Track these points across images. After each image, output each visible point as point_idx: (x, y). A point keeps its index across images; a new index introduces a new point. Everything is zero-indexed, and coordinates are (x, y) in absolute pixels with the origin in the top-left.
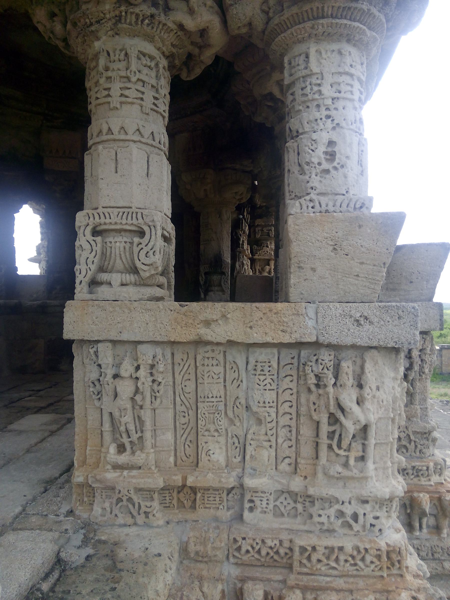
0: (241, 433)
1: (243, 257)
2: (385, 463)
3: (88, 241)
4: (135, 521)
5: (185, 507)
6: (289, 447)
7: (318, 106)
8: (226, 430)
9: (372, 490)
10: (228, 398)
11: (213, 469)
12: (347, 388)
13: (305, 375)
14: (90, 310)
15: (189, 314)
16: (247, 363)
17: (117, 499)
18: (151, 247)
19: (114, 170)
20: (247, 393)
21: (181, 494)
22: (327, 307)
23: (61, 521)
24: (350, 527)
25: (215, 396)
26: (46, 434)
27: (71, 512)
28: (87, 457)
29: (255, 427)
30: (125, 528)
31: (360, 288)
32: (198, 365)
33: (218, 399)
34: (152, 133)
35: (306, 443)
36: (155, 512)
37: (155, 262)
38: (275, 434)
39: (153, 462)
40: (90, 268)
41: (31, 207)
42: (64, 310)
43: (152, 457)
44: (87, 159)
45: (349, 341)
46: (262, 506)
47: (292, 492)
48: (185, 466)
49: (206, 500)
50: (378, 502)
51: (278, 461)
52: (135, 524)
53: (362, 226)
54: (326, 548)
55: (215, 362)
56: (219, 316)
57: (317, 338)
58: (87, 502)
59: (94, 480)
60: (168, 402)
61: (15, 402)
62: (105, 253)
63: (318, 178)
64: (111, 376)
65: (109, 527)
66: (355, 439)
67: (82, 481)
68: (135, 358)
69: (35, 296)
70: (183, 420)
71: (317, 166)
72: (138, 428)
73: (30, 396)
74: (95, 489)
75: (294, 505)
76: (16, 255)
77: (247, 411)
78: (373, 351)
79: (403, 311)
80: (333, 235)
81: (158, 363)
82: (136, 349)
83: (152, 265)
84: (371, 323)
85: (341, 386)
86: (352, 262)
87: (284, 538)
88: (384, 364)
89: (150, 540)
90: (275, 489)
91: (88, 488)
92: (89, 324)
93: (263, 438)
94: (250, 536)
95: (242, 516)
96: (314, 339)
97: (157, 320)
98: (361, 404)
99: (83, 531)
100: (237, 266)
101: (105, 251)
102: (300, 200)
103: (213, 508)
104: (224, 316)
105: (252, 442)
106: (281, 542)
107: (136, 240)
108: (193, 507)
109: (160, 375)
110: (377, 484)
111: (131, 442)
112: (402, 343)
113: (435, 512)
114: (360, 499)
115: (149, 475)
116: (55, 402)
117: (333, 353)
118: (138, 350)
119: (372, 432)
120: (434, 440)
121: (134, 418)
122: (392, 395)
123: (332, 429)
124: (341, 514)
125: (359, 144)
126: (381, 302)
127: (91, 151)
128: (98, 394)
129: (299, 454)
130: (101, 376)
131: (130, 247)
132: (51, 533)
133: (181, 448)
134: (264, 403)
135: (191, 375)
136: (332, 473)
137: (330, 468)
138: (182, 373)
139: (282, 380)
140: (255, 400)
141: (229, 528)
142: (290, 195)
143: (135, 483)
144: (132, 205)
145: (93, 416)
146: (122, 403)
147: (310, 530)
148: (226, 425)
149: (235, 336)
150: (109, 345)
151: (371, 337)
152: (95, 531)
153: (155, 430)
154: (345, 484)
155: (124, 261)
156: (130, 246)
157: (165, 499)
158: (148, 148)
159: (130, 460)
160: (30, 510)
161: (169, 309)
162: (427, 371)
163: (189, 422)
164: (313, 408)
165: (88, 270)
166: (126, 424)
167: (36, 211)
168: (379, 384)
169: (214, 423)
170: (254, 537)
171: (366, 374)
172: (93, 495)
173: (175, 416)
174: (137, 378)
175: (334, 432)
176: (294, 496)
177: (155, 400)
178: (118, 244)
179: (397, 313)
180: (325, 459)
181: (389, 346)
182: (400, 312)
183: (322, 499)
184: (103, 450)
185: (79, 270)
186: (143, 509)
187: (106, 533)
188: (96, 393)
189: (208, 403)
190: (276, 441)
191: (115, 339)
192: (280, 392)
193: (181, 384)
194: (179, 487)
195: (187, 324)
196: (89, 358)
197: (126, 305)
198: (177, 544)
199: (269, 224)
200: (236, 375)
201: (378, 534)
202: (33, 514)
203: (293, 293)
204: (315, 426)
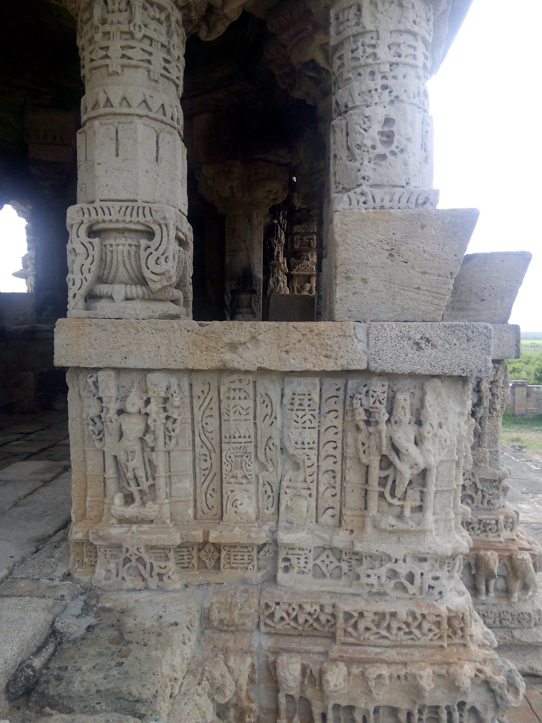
0: (274, 480)
1: (278, 272)
2: (447, 514)
4: (147, 584)
5: (206, 567)
6: (333, 496)
7: (372, 73)
9: (433, 546)
10: (259, 438)
11: (241, 522)
12: (404, 425)
13: (353, 410)
15: (210, 335)
16: (282, 396)
20: (282, 432)
23: (56, 586)
24: (405, 589)
25: (242, 436)
26: (38, 484)
27: (68, 576)
29: (291, 472)
31: (421, 304)
32: (222, 398)
33: (247, 440)
36: (170, 574)
37: (168, 271)
39: (168, 515)
40: (85, 277)
43: (166, 509)
44: (80, 138)
45: (406, 368)
46: (299, 565)
47: (336, 548)
48: (207, 519)
50: (439, 559)
52: (147, 588)
53: (426, 226)
54: (375, 614)
55: (243, 395)
58: (88, 563)
59: (96, 536)
60: (185, 442)
62: (104, 259)
63: (372, 165)
65: (115, 592)
66: (411, 486)
67: (82, 538)
68: (144, 389)
70: (204, 465)
71: (370, 150)
73: (18, 440)
74: (98, 548)
75: (338, 564)
77: (282, 453)
78: (435, 380)
79: (473, 332)
80: (389, 237)
81: (172, 395)
82: (146, 378)
83: (164, 274)
84: (434, 346)
85: (396, 422)
86: (412, 271)
87: (326, 603)
88: (448, 397)
89: (165, 606)
90: (315, 545)
91: (89, 547)
92: (86, 348)
93: (300, 485)
94: (285, 600)
95: (275, 577)
96: (364, 366)
98: (419, 444)
99: (83, 597)
100: (271, 282)
101: (104, 256)
102: (349, 193)
103: (241, 568)
105: (287, 490)
106: (322, 607)
107: (144, 242)
108: (217, 567)
109: (175, 411)
110: (437, 539)
111: (140, 491)
112: (471, 371)
113: (505, 573)
114: (416, 556)
115: (164, 530)
116: (49, 447)
117: (386, 383)
118: (147, 380)
119: (432, 478)
121: (144, 462)
122: (457, 433)
123: (384, 474)
124: (394, 574)
125: (423, 123)
128: (100, 433)
129: (345, 504)
130: (102, 411)
132: (44, 600)
133: (201, 498)
134: (303, 443)
137: (381, 520)
138: (203, 408)
139: (325, 417)
140: (292, 441)
141: (259, 592)
146: (129, 444)
148: (257, 470)
149: (268, 362)
150: (112, 373)
151: (433, 364)
152: (98, 598)
153: (170, 477)
154: (399, 539)
155: (129, 269)
156: (136, 250)
158: (157, 125)
159: (140, 513)
160: (17, 574)
161: (185, 329)
162: (498, 407)
163: (211, 467)
164: (361, 449)
165: (84, 280)
166: (134, 469)
167: (21, 213)
168: (442, 420)
169: (242, 468)
170: (290, 602)
172: (95, 554)
173: (194, 460)
174: (147, 414)
175: (386, 478)
176: (337, 553)
177: (170, 440)
178: (120, 247)
180: (376, 510)
181: (455, 374)
182: (470, 333)
183: (371, 557)
184: (106, 501)
185: (72, 281)
186: (156, 570)
187: (111, 599)
188: (97, 432)
189: (235, 445)
190: (317, 488)
191: (119, 367)
192: (322, 430)
194: (199, 544)
195: (209, 348)
196: (86, 390)
197: (132, 325)
199: (310, 232)
201: (438, 597)
202: (22, 578)
203: (339, 309)
204: (364, 472)
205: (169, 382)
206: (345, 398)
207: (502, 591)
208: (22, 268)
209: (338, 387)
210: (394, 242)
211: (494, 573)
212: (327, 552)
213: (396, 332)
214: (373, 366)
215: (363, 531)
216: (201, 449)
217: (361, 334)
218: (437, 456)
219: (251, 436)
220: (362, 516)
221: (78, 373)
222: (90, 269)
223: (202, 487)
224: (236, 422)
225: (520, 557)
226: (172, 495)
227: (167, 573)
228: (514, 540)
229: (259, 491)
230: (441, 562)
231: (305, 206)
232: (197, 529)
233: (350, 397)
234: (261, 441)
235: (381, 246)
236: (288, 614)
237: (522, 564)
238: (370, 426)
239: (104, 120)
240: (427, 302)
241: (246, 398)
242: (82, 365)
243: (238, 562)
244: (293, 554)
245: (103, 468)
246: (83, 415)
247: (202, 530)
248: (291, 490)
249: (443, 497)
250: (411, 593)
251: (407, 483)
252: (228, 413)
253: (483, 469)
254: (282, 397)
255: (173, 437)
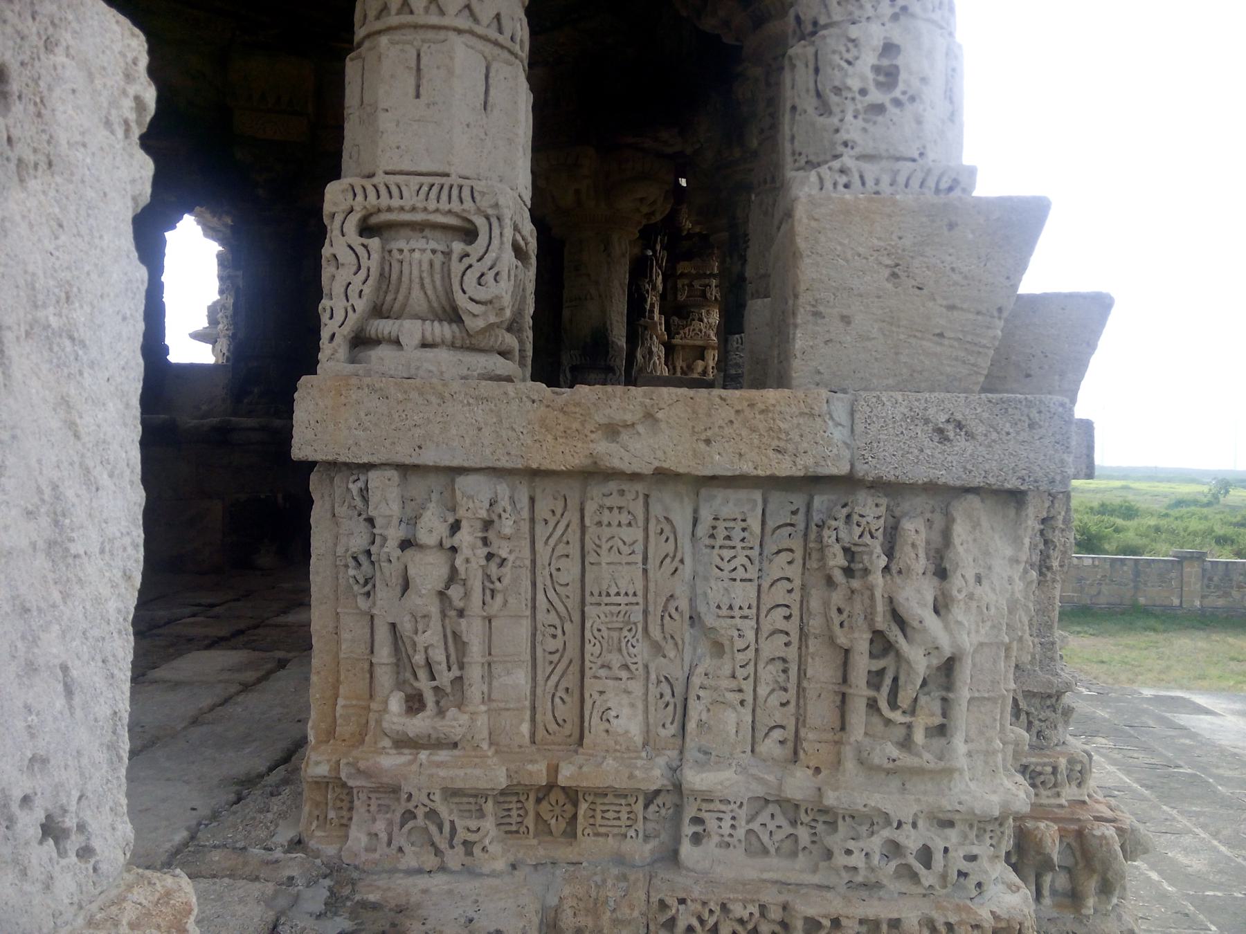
0: (678, 674)
1: (651, 338)
2: (989, 741)
3: (350, 247)
4: (443, 861)
5: (551, 833)
6: (783, 705)
8: (646, 667)
9: (964, 797)
10: (651, 596)
11: (616, 750)
12: (914, 577)
13: (822, 550)
14: (354, 397)
15: (573, 409)
16: (695, 522)
17: (404, 813)
18: (489, 264)
19: (412, 91)
20: (693, 588)
21: (545, 804)
22: (874, 400)
23: (277, 861)
24: (914, 877)
25: (623, 592)
26: (233, 689)
27: (298, 844)
28: (338, 722)
29: (708, 660)
30: (419, 876)
31: (945, 362)
32: (587, 522)
33: (631, 599)
34: (498, 17)
35: (820, 696)
36: (487, 842)
37: (499, 297)
38: (752, 675)
39: (485, 734)
40: (353, 306)
41: (199, 223)
42: (296, 395)
43: (482, 722)
44: (352, 68)
45: (921, 474)
46: (721, 831)
47: (788, 801)
48: (554, 744)
49: (599, 816)
50: (976, 823)
51: (757, 734)
52: (443, 869)
53: (957, 225)
54: (861, 922)
55: (625, 518)
56: (639, 415)
57: (852, 465)
58: (335, 821)
59: (353, 771)
60: (519, 602)
61: (159, 627)
62: (387, 275)
63: (860, 123)
64: (396, 543)
65: (384, 875)
66: (926, 689)
67: (326, 774)
68: (450, 505)
69: (204, 408)
70: (552, 645)
71: (858, 97)
72: (453, 658)
73: (194, 615)
74: (355, 791)
75: (791, 831)
76: (167, 320)
77: (692, 625)
78: (970, 497)
79: (1040, 412)
80: (893, 243)
81: (500, 516)
82: (453, 485)
83: (491, 302)
84: (970, 436)
85: (900, 572)
86: (931, 304)
87: (770, 901)
88: (992, 528)
89: (477, 901)
90: (750, 795)
91: (338, 790)
92: (349, 428)
93: (726, 683)
94: (696, 895)
95: (676, 853)
96: (844, 469)
97: (501, 421)
98: (943, 612)
99: (328, 882)
100: (639, 356)
101: (387, 269)
102: (819, 169)
103: (614, 835)
104: (649, 416)
105: (701, 693)
106: (763, 908)
107: (458, 247)
108: (571, 833)
109: (505, 544)
110: (973, 785)
111: (436, 689)
112: (1036, 481)
113: (1069, 862)
114: (934, 818)
115: (477, 760)
116: (249, 628)
117: (884, 501)
118: (456, 487)
119: (965, 673)
120: (1068, 712)
121: (445, 636)
122: (1008, 595)
123: (877, 665)
124: (895, 848)
125: (947, 54)
126: (991, 391)
127: (363, 49)
128: (366, 583)
129: (804, 721)
130: (373, 543)
131: (444, 263)
132: (257, 885)
133: (544, 705)
134: (731, 608)
135: (571, 545)
136: (877, 761)
137: (873, 749)
138: (552, 542)
139: (771, 561)
140: (711, 603)
141: (648, 878)
142: (795, 161)
143: (443, 778)
144: (452, 170)
145: (353, 632)
146: (419, 601)
147: (826, 884)
148: (646, 655)
149: (673, 458)
150: (394, 474)
151: (969, 467)
152: (353, 884)
153: (489, 665)
154: (904, 785)
155: (430, 292)
156: (443, 260)
157: (509, 816)
158: (488, 49)
159: (434, 728)
160: (204, 837)
161: (528, 397)
162: (1055, 564)
163: (564, 648)
164: (836, 619)
165: (350, 310)
166: (426, 649)
167: (210, 231)
168: (981, 570)
169: (620, 650)
170: (703, 898)
171: (955, 547)
172: (348, 805)
173: (534, 635)
174: (454, 549)
175: (881, 673)
176: (791, 809)
177: (492, 598)
178: (417, 255)
179: (1028, 416)
180: (862, 731)
181: (1008, 486)
182: (1034, 413)
183: (853, 817)
184: (374, 706)
185: (328, 311)
186: (462, 835)
187: (378, 888)
188: (362, 581)
189: (609, 608)
190: (755, 690)
191: (407, 462)
192: (765, 585)
193: (550, 565)
194: (540, 788)
195: (569, 432)
196: (346, 504)
197: (434, 388)
198: (537, 912)
200: (670, 546)
201: (974, 893)
202: (215, 847)
203: (799, 368)
204: (839, 661)
205: (496, 493)
206: (807, 528)
207: (1065, 895)
208: (207, 325)
209: (794, 508)
210: (900, 251)
211: (1052, 860)
212: (772, 808)
213: (903, 409)
214: (861, 470)
215: (837, 770)
216: (546, 616)
217: (841, 413)
218: (973, 635)
219: (638, 593)
220: (836, 743)
221: (332, 474)
222: (361, 291)
223: (546, 685)
224: (612, 566)
225: (1097, 833)
226: (493, 697)
227: (480, 841)
228: (1084, 802)
229: (650, 694)
230: (979, 829)
231: (697, 230)
232: (536, 762)
233: (817, 526)
234: (655, 603)
235: (877, 259)
236: (702, 922)
237: (1101, 846)
238: (853, 577)
239: (397, 36)
240: (956, 359)
241: (630, 524)
242: (342, 459)
243: (610, 823)
244: (709, 811)
245: (369, 645)
246: (338, 550)
247: (546, 762)
248: (708, 692)
249: (983, 709)
250: (927, 884)
251: (919, 682)
252: (598, 550)
253: (1029, 674)
254: (695, 525)
255: (499, 591)
